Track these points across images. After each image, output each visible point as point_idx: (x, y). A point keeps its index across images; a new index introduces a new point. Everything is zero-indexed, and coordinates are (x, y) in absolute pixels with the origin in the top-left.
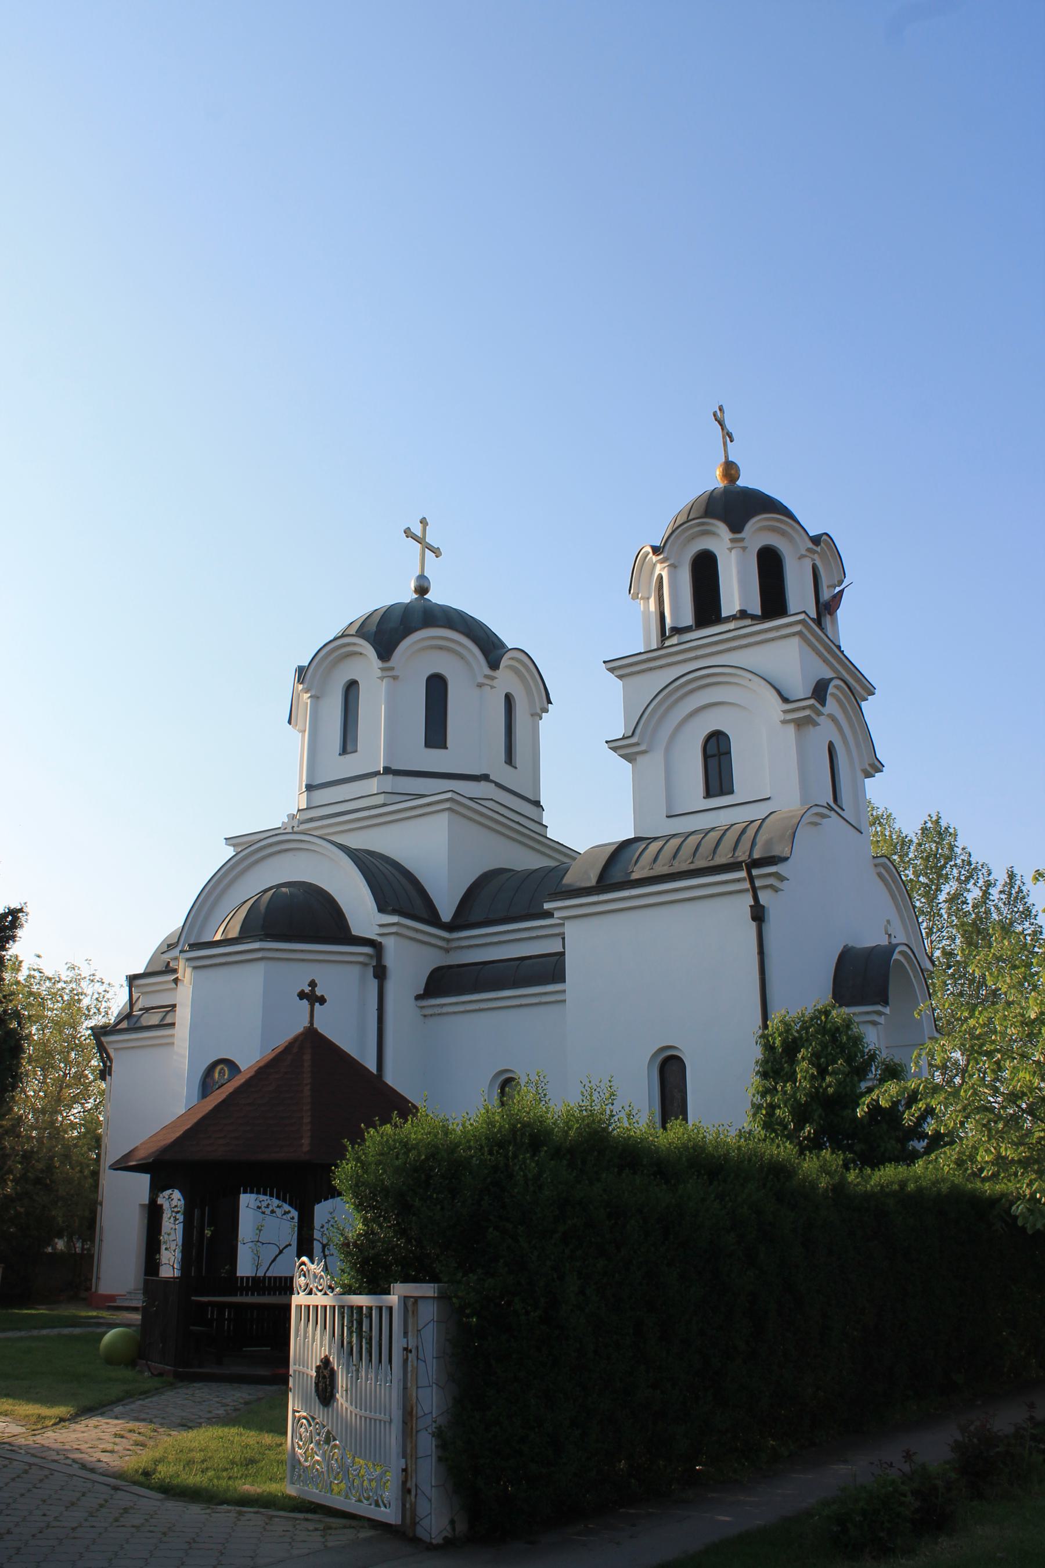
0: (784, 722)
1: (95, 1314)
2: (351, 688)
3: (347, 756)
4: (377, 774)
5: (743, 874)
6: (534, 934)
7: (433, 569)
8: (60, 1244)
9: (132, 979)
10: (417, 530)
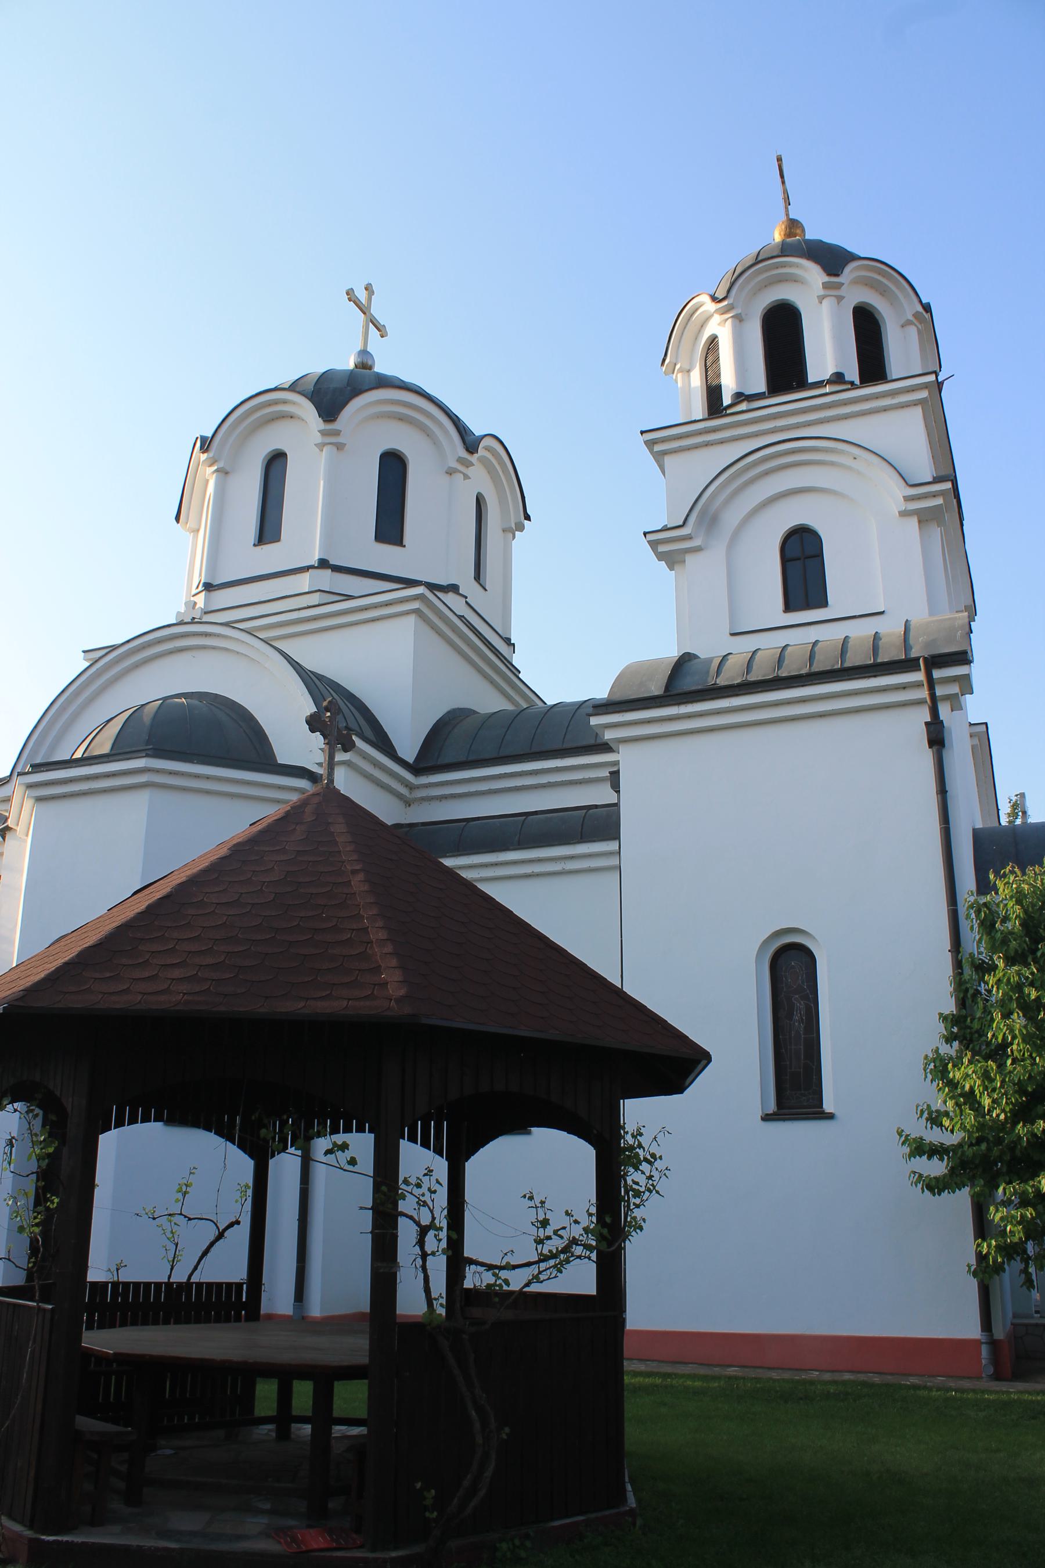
0: (904, 514)
2: (276, 462)
3: (265, 547)
4: (308, 568)
5: (920, 676)
7: (376, 345)
10: (362, 295)
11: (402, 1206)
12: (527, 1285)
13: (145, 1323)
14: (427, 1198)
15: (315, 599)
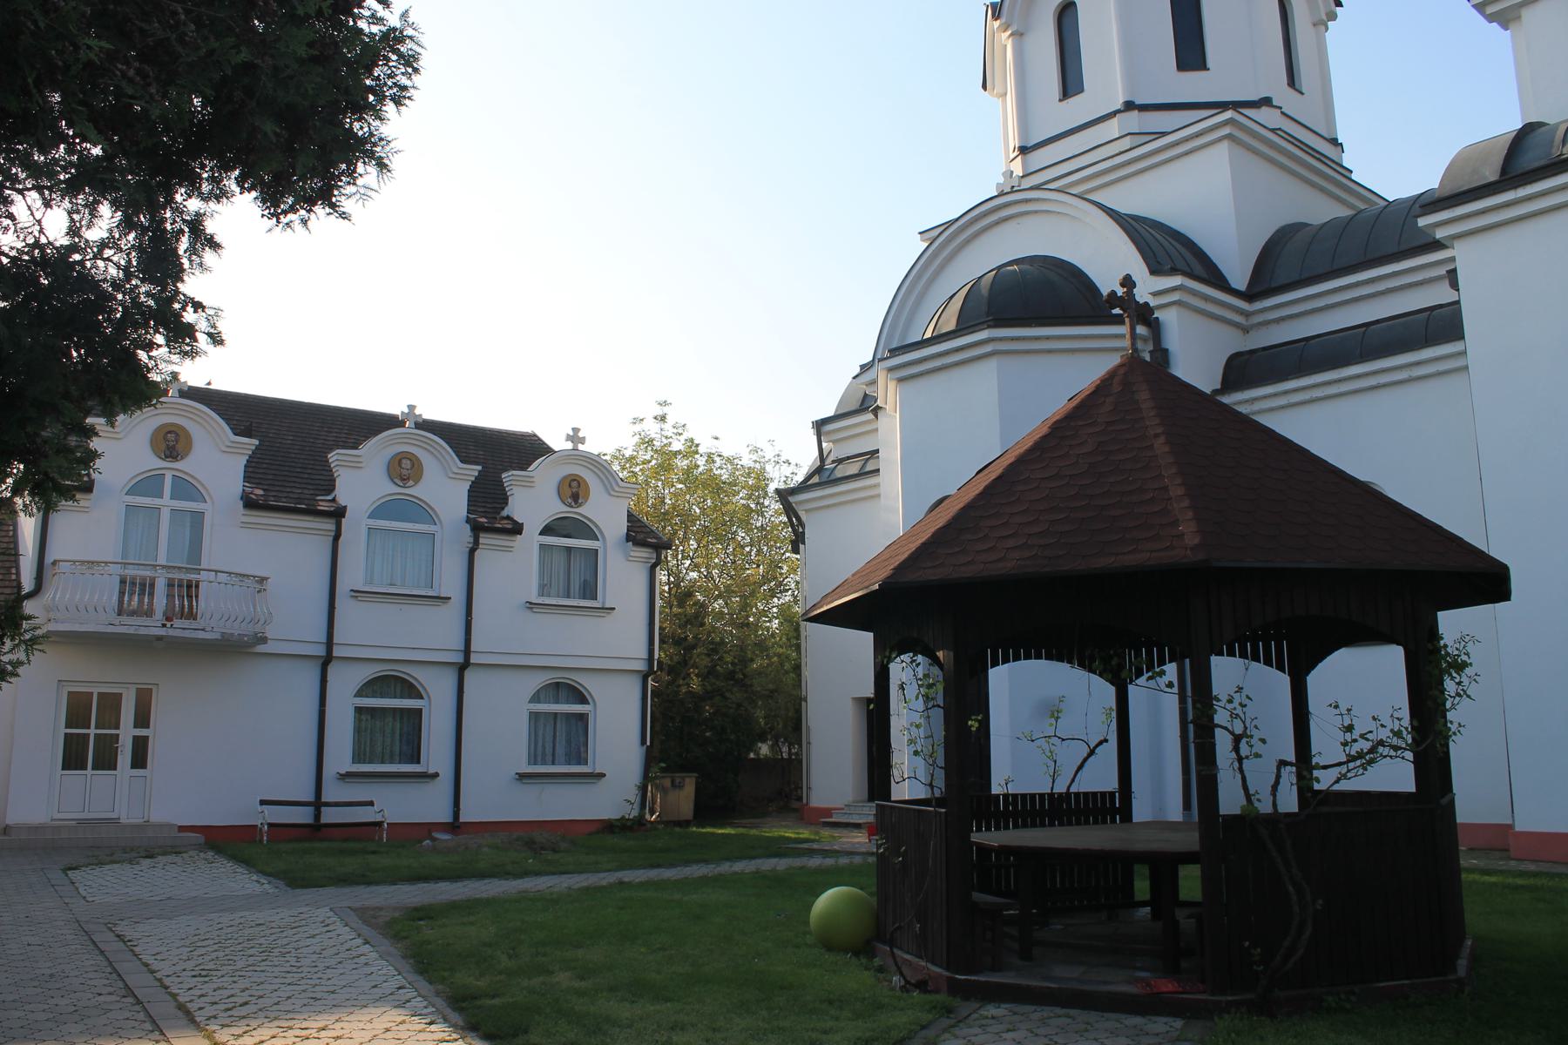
1: (805, 834)
6: (1381, 286)
8: (765, 749)
9: (820, 426)
11: (1218, 719)
12: (1337, 781)
13: (1034, 825)
14: (1239, 711)
15: (1126, 143)
